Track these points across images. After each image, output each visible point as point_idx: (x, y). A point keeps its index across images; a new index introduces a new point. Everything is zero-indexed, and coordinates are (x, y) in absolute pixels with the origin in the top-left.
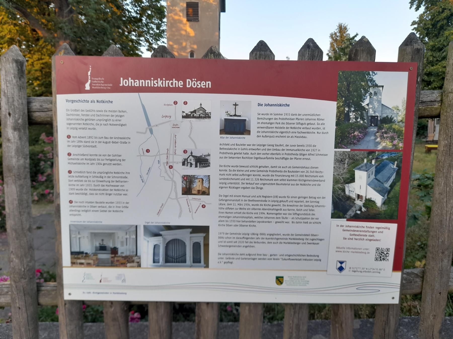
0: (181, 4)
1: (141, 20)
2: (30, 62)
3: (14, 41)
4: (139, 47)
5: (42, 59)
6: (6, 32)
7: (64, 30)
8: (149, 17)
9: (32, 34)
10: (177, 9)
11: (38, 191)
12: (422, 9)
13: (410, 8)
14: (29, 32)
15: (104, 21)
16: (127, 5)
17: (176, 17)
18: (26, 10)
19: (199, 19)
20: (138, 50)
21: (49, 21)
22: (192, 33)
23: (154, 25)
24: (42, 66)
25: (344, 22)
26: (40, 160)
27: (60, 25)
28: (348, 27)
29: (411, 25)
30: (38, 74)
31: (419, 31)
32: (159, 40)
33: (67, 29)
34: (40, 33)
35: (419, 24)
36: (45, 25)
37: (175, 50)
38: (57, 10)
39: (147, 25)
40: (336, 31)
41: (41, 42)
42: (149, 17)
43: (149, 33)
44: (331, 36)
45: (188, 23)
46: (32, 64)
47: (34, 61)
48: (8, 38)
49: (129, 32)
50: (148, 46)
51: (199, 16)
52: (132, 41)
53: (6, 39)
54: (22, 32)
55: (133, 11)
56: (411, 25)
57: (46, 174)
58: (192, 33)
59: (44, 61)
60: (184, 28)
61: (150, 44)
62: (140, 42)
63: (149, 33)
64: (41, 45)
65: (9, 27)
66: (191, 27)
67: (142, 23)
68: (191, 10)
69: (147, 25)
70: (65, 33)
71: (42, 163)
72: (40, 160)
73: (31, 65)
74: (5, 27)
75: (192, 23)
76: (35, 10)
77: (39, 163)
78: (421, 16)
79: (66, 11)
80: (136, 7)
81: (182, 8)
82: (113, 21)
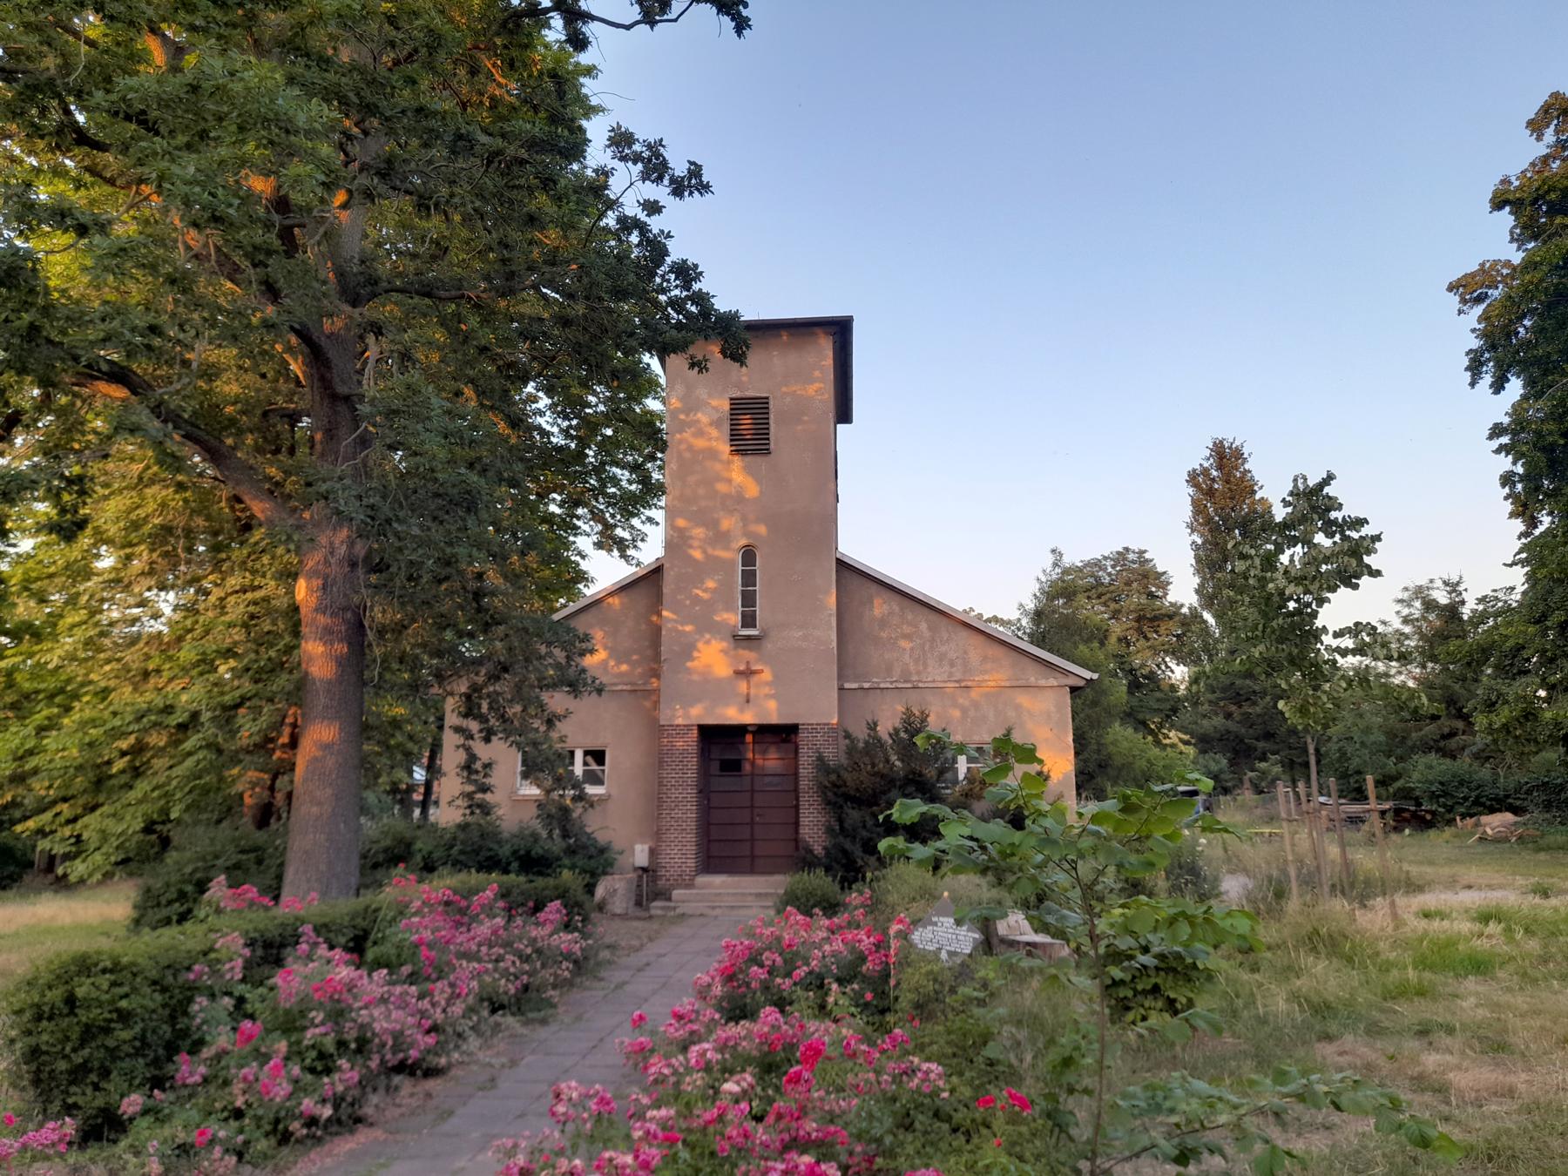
0: (714, 403)
1: (580, 456)
2: (212, 598)
3: (172, 535)
4: (571, 538)
5: (254, 588)
6: (151, 507)
7: (336, 500)
8: (607, 446)
9: (232, 508)
10: (702, 417)
11: (167, 1131)
12: (1515, 388)
13: (1473, 384)
14: (223, 504)
15: (471, 466)
16: (541, 413)
17: (700, 443)
18: (222, 442)
19: (772, 446)
20: (567, 545)
21: (287, 473)
22: (752, 490)
23: (623, 468)
24: (251, 609)
25: (1231, 434)
26: (191, 990)
27: (324, 487)
28: (1246, 451)
29: (1491, 438)
30: (238, 635)
31: (1523, 455)
32: (637, 515)
33: (345, 501)
34: (259, 508)
35: (1515, 433)
36: (277, 484)
37: (696, 543)
38: (318, 436)
39: (598, 470)
40: (1206, 465)
41: (257, 535)
42: (607, 446)
43: (605, 495)
44: (1193, 478)
45: (738, 461)
46: (221, 605)
47: (228, 595)
48: (155, 526)
49: (542, 496)
50: (601, 533)
51: (772, 436)
52: (549, 519)
53: (147, 529)
54: (203, 505)
55: (555, 430)
56: (1491, 438)
57: (206, 1053)
58: (752, 490)
59: (259, 594)
60: (725, 474)
61: (608, 527)
62: (579, 523)
63: (605, 495)
64: (256, 543)
65: (164, 493)
66: (748, 470)
67: (584, 465)
68: (746, 421)
69: (598, 470)
70: (338, 513)
71: (201, 1001)
72: (191, 990)
73: (215, 606)
74: (149, 491)
75: (748, 459)
76: (249, 440)
77: (190, 1000)
78: (1517, 410)
79: (347, 441)
80: (566, 417)
81: (716, 416)
82: (498, 463)
